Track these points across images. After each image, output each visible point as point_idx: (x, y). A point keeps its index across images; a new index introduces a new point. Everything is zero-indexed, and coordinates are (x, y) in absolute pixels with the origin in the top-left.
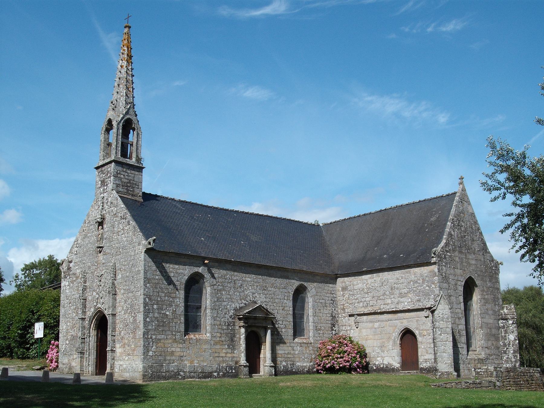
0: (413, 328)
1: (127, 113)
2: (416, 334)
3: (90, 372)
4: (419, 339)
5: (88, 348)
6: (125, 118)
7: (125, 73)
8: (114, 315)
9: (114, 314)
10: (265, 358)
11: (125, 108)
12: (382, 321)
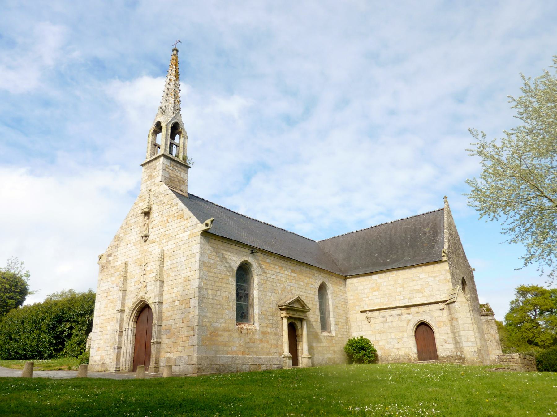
0: (427, 319)
3: (127, 369)
5: (126, 341)
6: (173, 122)
7: (174, 85)
8: (161, 303)
9: (161, 302)
10: (302, 349)
11: (173, 113)
12: (395, 316)
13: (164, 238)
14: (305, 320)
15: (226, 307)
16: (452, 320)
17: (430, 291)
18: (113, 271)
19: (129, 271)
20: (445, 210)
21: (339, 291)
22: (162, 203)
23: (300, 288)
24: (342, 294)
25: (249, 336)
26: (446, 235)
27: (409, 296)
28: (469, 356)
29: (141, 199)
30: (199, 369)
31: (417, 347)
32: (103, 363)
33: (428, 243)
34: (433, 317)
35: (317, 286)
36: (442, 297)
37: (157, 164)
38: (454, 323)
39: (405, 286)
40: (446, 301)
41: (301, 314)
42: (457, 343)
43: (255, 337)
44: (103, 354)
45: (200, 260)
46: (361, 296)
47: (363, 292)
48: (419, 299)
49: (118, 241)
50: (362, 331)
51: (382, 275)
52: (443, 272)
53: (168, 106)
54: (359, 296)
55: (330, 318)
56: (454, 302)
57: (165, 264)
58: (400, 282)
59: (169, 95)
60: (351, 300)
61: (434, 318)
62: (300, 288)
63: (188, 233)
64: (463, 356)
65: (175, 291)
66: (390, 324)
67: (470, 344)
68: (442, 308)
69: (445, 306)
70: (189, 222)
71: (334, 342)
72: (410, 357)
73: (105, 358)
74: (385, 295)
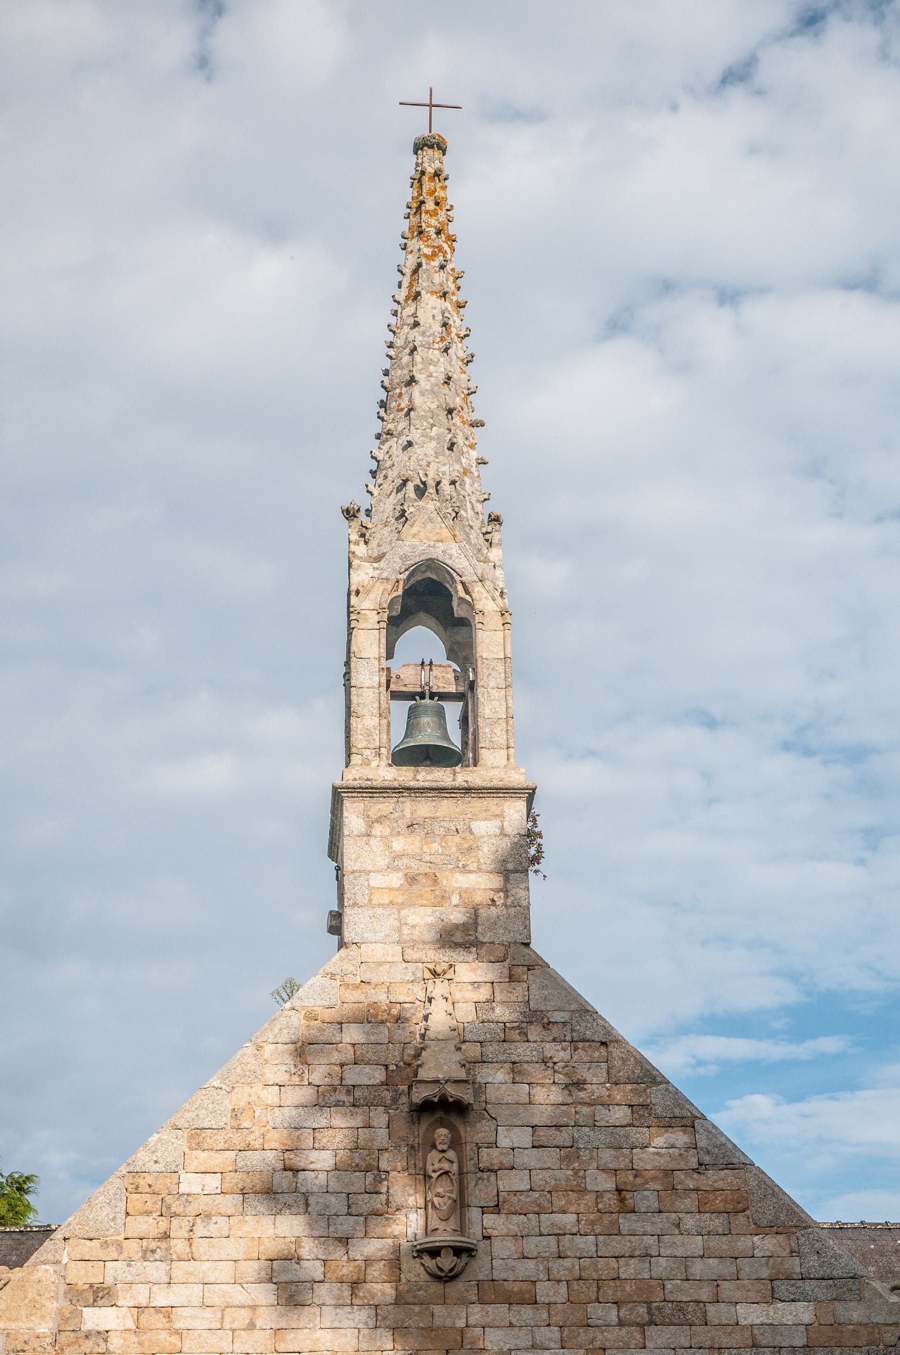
63: (804, 1313)
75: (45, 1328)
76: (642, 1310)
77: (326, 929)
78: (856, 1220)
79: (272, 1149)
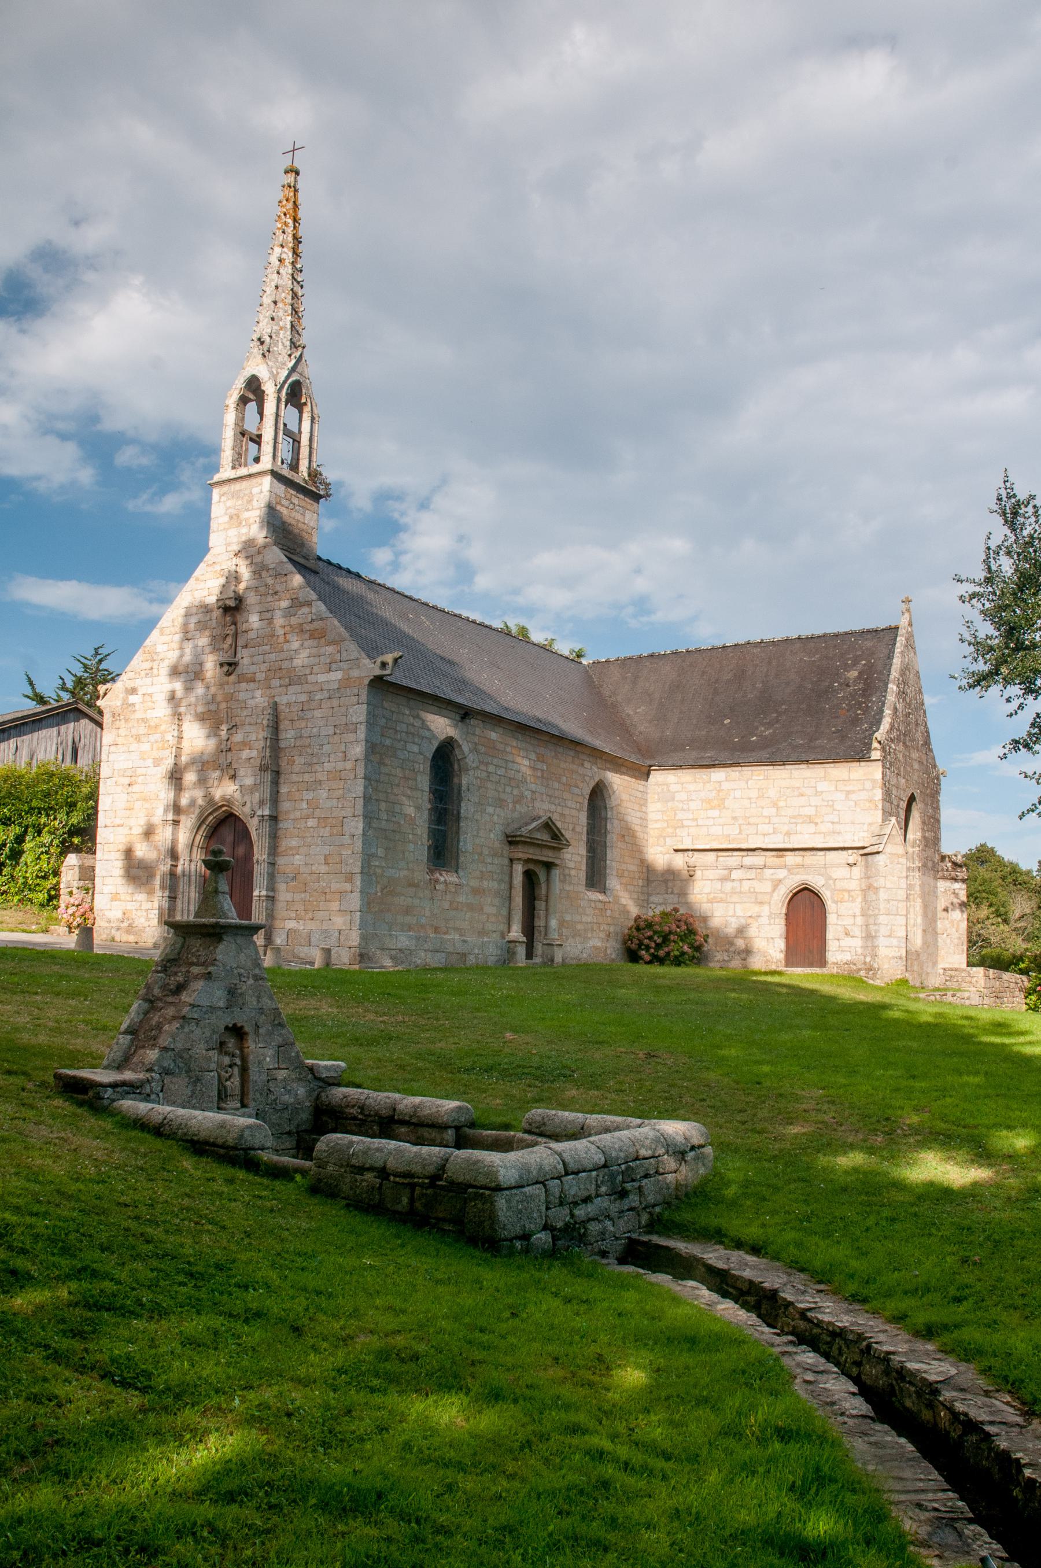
0: (817, 882)
1: (293, 370)
2: (544, 886)
4: (830, 906)
6: (290, 381)
13: (278, 675)
14: (557, 865)
15: (410, 836)
16: (869, 889)
17: (833, 823)
18: (142, 730)
19: (184, 735)
20: (900, 632)
21: (630, 801)
22: (271, 591)
23: (550, 796)
24: (636, 807)
25: (448, 897)
26: (891, 698)
27: (785, 828)
28: (886, 966)
29: (210, 569)
30: (361, 955)
31: (787, 938)
32: (130, 925)
33: (848, 711)
34: (830, 878)
35: (587, 791)
36: (856, 838)
37: (256, 490)
38: (871, 896)
39: (782, 804)
40: (864, 848)
41: (550, 853)
42: (869, 937)
43: (460, 899)
44: (129, 908)
45: (367, 741)
46: (680, 815)
47: (685, 807)
48: (807, 836)
49: (153, 660)
50: (672, 893)
51: (734, 773)
52: (868, 785)
53: (278, 335)
54: (675, 814)
55: (605, 861)
56: (878, 853)
57: (282, 736)
58: (772, 793)
59: (280, 305)
60: (656, 821)
61: (831, 882)
62: (550, 796)
63: (339, 675)
64: (876, 966)
65: (306, 797)
66: (736, 884)
67: (895, 942)
68: (851, 861)
69: (860, 858)
70: (340, 652)
71: (609, 913)
72: (769, 958)
73: (134, 916)
74: (735, 818)
75: (119, 703)
76: (287, 680)
77: (258, 374)
78: (821, 633)
79: (31, 683)
